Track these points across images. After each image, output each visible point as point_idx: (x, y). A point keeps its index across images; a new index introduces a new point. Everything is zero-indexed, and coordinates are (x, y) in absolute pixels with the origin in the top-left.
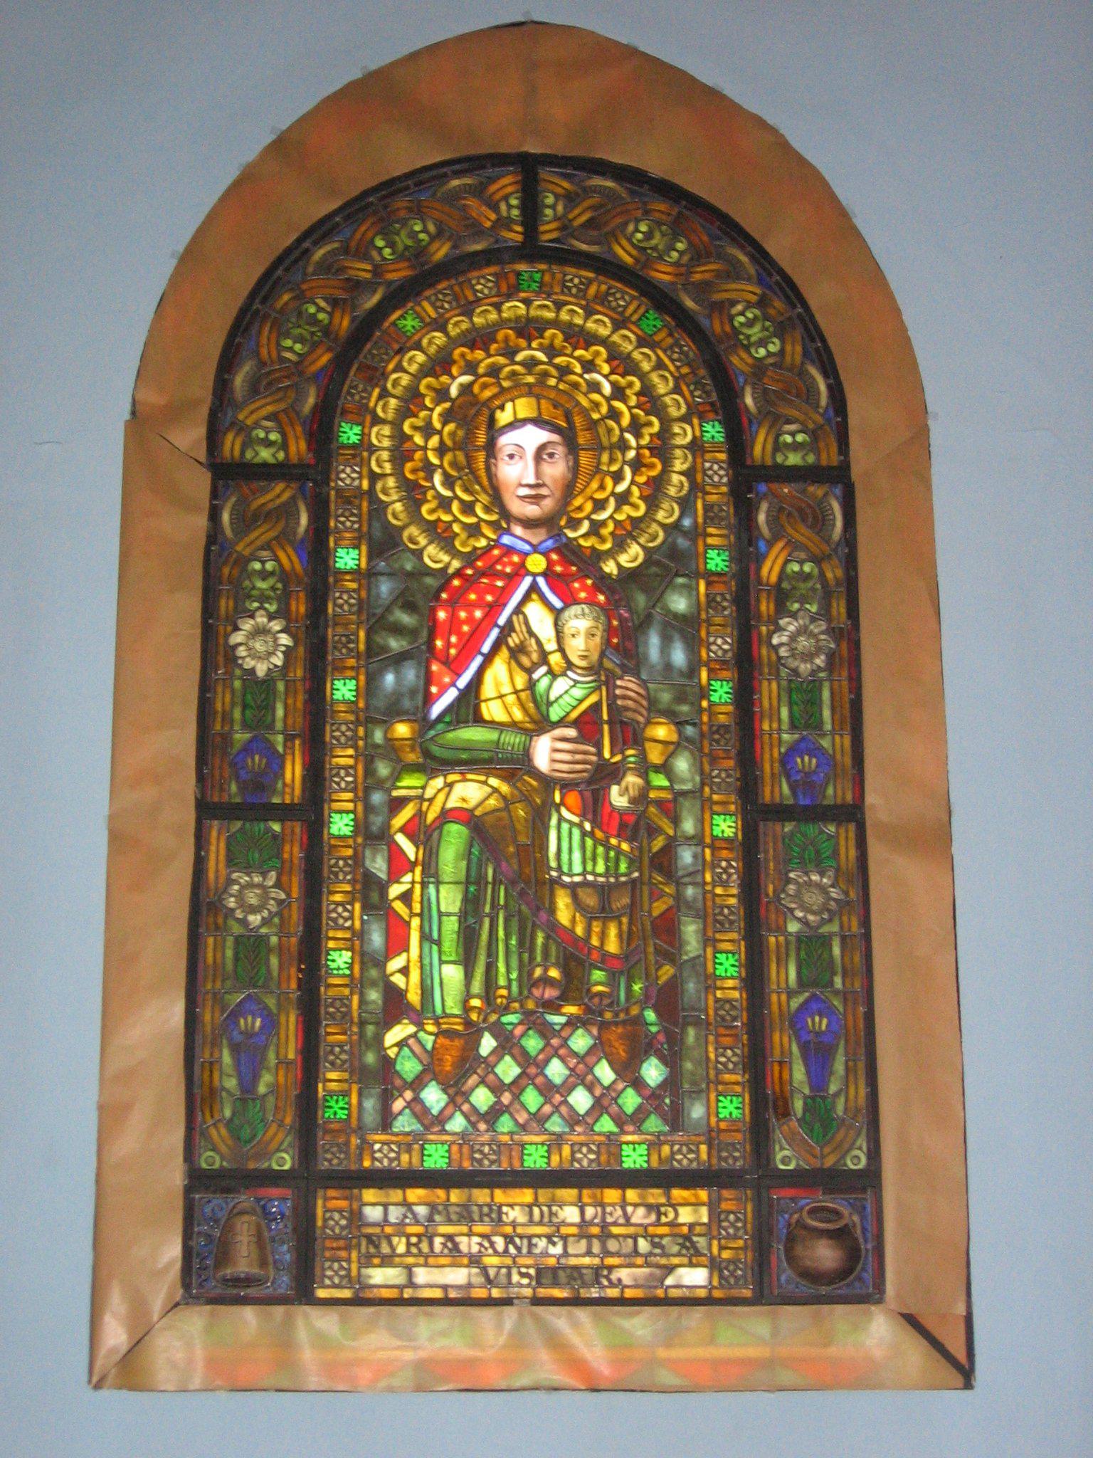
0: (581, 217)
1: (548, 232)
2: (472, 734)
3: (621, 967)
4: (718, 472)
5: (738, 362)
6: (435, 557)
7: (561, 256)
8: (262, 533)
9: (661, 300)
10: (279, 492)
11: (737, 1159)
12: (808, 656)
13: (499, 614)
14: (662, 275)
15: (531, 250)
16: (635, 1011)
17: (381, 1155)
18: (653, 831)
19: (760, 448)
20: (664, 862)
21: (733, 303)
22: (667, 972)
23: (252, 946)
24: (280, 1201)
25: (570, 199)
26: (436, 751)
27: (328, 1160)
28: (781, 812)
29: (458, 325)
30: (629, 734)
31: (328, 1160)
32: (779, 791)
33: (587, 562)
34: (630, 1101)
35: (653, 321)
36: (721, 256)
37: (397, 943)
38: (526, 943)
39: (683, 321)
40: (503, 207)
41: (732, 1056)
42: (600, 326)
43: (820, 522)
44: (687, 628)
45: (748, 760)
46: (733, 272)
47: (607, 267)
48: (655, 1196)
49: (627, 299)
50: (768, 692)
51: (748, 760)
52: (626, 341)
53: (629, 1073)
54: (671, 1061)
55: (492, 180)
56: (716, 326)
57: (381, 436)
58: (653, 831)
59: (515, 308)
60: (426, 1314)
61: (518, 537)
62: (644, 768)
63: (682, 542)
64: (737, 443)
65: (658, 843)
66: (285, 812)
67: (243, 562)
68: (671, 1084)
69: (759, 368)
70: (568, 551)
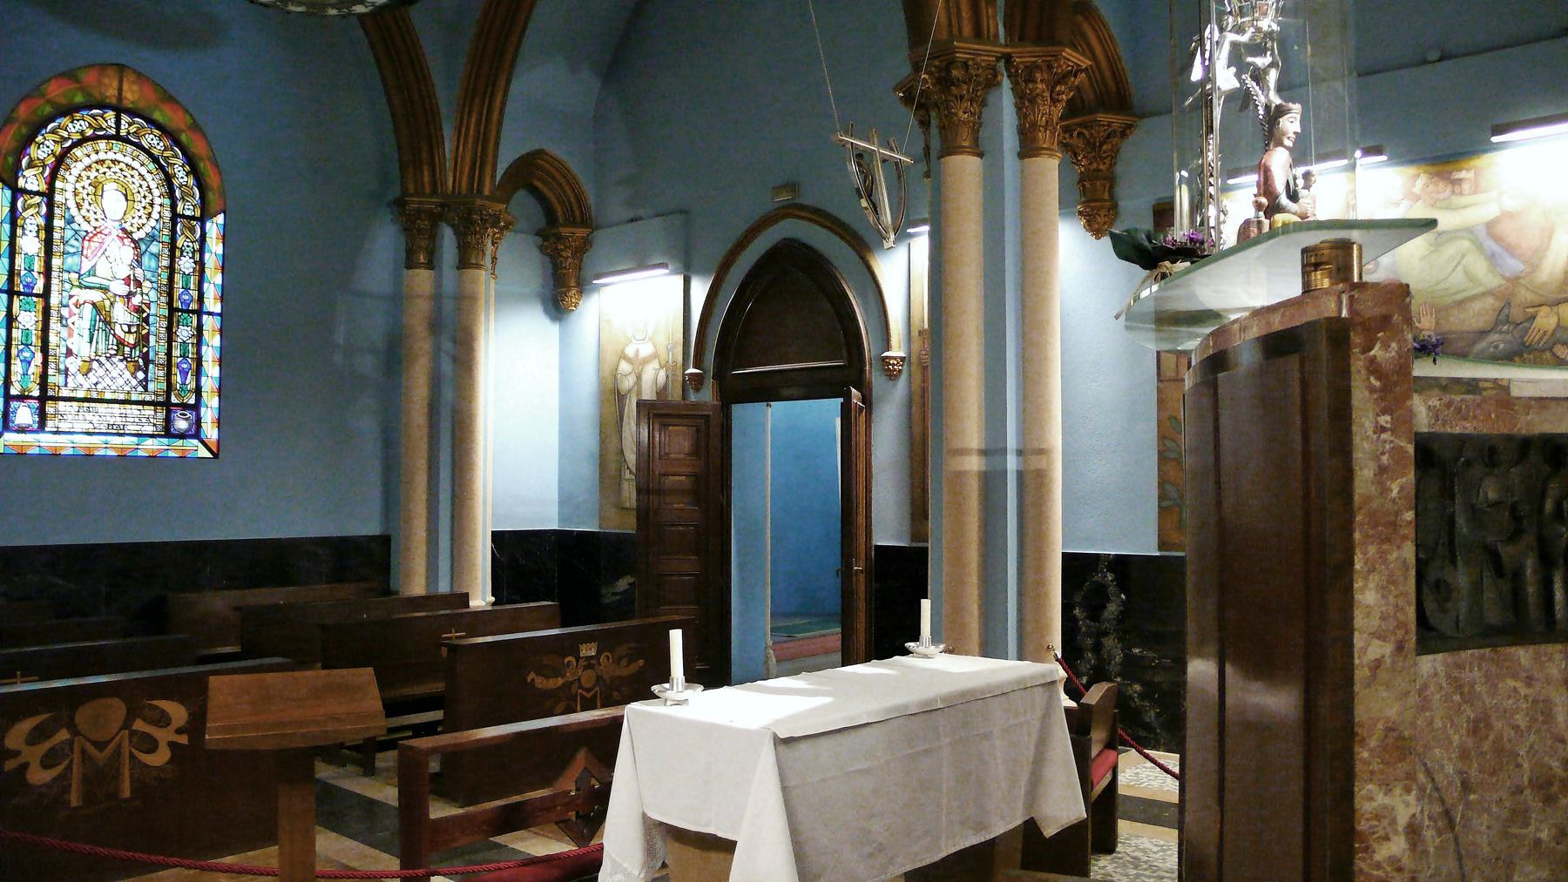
0: (133, 129)
1: (123, 133)
2: (91, 279)
3: (133, 347)
4: (167, 214)
5: (175, 182)
6: (85, 226)
7: (126, 140)
8: (32, 211)
9: (155, 160)
10: (37, 199)
11: (161, 399)
12: (188, 269)
13: (1353, 277)
14: (155, 152)
15: (117, 137)
16: (136, 359)
17: (64, 393)
18: (144, 311)
19: (179, 209)
20: (146, 320)
21: (175, 164)
22: (145, 350)
23: (26, 332)
24: (35, 404)
25: (130, 125)
26: (83, 282)
27: (50, 393)
28: (178, 310)
29: (94, 157)
30: (139, 284)
31: (50, 393)
32: (178, 304)
33: (129, 234)
34: (134, 382)
35: (152, 166)
36: (172, 150)
37: (71, 335)
38: (107, 339)
39: (161, 167)
40: (109, 121)
41: (161, 373)
42: (136, 164)
43: (192, 231)
44: (157, 256)
45: (170, 295)
46: (176, 156)
47: (139, 146)
48: (140, 407)
49: (143, 157)
50: (178, 277)
51: (170, 295)
52: (143, 171)
53: (134, 375)
54: (146, 372)
55: (106, 113)
56: (170, 170)
57: (70, 187)
58: (144, 311)
59: (111, 155)
60: (946, 379)
61: (109, 224)
62: (142, 294)
63: (156, 233)
64: (173, 207)
65: (145, 315)
66: (37, 296)
67: (25, 219)
68: (146, 379)
69: (181, 186)
70: (124, 230)
